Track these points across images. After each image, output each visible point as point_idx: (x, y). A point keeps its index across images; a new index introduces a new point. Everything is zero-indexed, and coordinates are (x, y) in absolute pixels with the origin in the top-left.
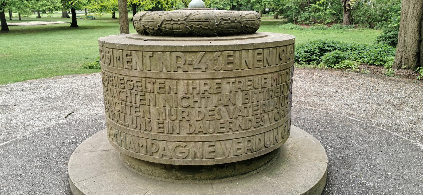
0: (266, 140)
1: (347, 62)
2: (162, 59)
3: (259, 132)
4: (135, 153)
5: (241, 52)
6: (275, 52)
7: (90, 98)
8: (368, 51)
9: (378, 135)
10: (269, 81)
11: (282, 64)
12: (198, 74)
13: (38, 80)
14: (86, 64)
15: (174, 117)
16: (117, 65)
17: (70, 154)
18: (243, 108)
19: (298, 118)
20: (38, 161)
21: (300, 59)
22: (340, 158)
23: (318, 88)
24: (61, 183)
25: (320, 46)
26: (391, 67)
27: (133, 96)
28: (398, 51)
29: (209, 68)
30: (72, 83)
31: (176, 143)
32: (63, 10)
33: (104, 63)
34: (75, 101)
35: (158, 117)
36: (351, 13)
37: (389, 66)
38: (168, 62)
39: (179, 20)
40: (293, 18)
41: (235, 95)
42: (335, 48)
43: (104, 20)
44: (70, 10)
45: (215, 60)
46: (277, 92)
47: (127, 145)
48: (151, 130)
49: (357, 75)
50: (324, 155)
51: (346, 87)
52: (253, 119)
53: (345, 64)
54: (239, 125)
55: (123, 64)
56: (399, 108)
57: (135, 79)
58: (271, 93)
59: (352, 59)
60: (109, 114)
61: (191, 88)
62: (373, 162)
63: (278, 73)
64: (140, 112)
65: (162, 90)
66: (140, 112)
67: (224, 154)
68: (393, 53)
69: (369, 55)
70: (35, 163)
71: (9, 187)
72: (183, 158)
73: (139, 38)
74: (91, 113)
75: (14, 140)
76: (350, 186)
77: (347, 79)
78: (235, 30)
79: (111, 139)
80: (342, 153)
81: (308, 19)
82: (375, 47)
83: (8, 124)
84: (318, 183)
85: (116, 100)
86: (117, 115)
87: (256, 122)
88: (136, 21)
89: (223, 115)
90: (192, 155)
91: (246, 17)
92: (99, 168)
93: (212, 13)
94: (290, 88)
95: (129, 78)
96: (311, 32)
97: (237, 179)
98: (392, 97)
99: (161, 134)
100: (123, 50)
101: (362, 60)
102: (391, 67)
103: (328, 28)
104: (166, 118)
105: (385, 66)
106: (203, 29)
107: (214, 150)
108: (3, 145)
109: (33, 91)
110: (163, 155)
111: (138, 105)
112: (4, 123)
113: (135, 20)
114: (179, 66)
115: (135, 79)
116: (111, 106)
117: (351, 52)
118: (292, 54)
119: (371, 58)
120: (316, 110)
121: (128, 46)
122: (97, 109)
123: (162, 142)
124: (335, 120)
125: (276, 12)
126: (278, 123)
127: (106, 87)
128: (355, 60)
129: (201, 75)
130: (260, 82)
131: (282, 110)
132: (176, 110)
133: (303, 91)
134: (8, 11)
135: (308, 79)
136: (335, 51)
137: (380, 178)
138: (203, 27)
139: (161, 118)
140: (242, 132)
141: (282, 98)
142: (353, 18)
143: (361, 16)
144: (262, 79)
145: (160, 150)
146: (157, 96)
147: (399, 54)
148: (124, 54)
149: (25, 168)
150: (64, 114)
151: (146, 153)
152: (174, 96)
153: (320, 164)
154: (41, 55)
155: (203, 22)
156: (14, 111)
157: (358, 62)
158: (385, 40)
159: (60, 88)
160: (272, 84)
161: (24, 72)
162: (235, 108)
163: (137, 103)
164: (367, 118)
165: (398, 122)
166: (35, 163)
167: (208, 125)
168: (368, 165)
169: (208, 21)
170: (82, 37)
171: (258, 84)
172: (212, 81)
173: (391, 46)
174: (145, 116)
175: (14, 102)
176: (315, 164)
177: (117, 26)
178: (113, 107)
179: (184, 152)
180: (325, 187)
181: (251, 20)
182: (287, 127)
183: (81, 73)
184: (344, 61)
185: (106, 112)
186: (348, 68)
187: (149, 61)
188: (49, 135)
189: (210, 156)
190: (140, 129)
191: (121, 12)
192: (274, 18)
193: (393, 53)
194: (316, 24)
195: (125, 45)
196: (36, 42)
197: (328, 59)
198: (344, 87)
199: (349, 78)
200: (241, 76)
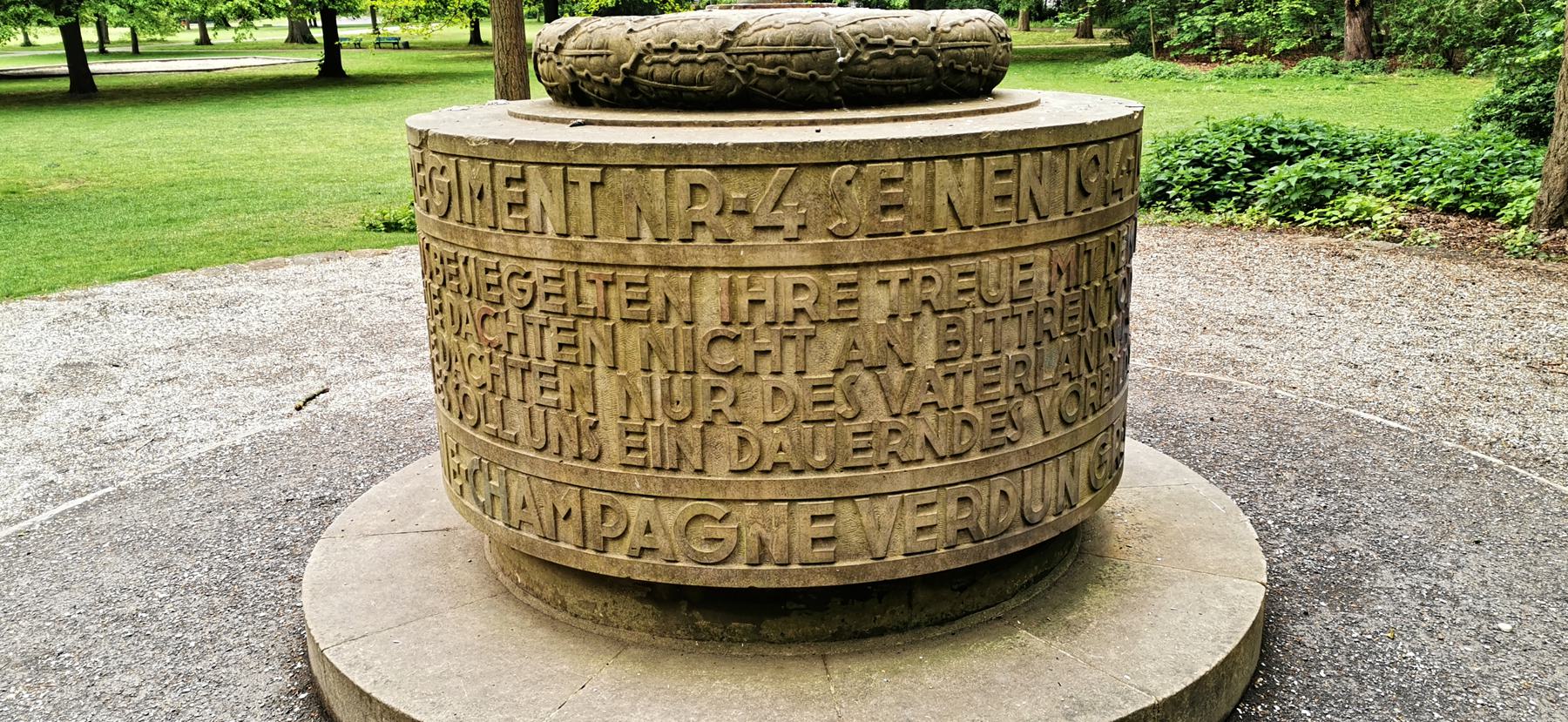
0: (1027, 497)
1: (1353, 201)
2: (635, 192)
3: (1001, 465)
4: (542, 540)
5: (932, 166)
6: (1064, 164)
7: (384, 340)
8: (1437, 159)
9: (1468, 478)
10: (1041, 275)
11: (1090, 209)
12: (773, 249)
13: (201, 274)
14: (374, 215)
15: (682, 411)
16: (473, 217)
17: (311, 542)
18: (940, 375)
19: (1159, 415)
20: (195, 567)
21: (1172, 193)
22: (1317, 566)
23: (1239, 302)
24: (279, 646)
25: (1251, 139)
26: (1527, 221)
27: (532, 333)
28: (1552, 158)
29: (810, 228)
30: (322, 282)
31: (689, 504)
32: (292, 15)
33: (428, 210)
34: (333, 350)
35: (625, 407)
36: (1376, 13)
37: (1518, 216)
38: (659, 206)
39: (700, 47)
40: (1149, 36)
41: (909, 327)
42: (1311, 147)
43: (439, 52)
44: (318, 16)
45: (833, 196)
46: (1071, 318)
47: (513, 511)
48: (599, 457)
49: (1393, 252)
50: (1254, 555)
51: (1347, 297)
52: (980, 419)
53: (1347, 210)
54: (926, 439)
55: (495, 215)
56: (1551, 377)
57: (539, 270)
58: (1047, 319)
59: (1374, 191)
60: (448, 396)
61: (743, 302)
62: (1444, 583)
63: (1073, 245)
64: (557, 389)
65: (639, 309)
66: (557, 389)
67: (869, 545)
68: (1534, 165)
69: (1441, 176)
70: (186, 575)
71: (93, 660)
72: (715, 560)
73: (554, 116)
74: (389, 392)
75: (110, 489)
76: (1351, 672)
77: (1352, 265)
78: (914, 83)
79: (455, 490)
80: (1323, 547)
81: (1209, 38)
82: (1464, 142)
83: (90, 433)
84: (1228, 657)
85: (472, 347)
86: (477, 400)
87: (988, 427)
88: (543, 54)
89: (864, 401)
90: (749, 548)
91: (955, 32)
92: (414, 594)
93: (826, 19)
94: (1122, 300)
95: (519, 263)
96: (1220, 88)
97: (918, 642)
98: (1525, 333)
99: (634, 472)
100: (494, 161)
101: (1413, 194)
102: (1527, 221)
103: (1286, 72)
104: (652, 414)
105: (1503, 214)
106: (791, 79)
107: (831, 530)
108: (72, 509)
109: (182, 314)
110: (643, 549)
111: (550, 363)
112: (75, 429)
113: (541, 50)
114: (702, 220)
115: (539, 270)
116: (454, 367)
117: (1372, 161)
118: (1129, 172)
119: (1449, 185)
120: (1230, 383)
121: (512, 147)
122: (410, 381)
123: (638, 501)
124: (1302, 424)
125: (1083, 12)
126: (1075, 434)
127: (435, 297)
128: (1388, 195)
129: (782, 254)
130: (1005, 279)
131: (1089, 385)
132: (688, 385)
133: (1179, 313)
134: (92, 20)
135: (1202, 267)
136: (1307, 161)
137: (1467, 643)
138: (791, 72)
139: (634, 414)
140: (936, 465)
141: (1088, 338)
142: (1383, 32)
143: (1412, 26)
144: (1012, 268)
145: (631, 529)
146: (619, 330)
147: (1556, 171)
148: (497, 177)
149: (150, 592)
150: (291, 397)
151: (580, 543)
152: (681, 333)
153: (1236, 586)
154: (213, 183)
155: (789, 56)
156: (112, 387)
157: (1398, 202)
158: (1507, 118)
159: (279, 301)
160: (1049, 287)
161: (151, 244)
162: (912, 376)
163: (547, 356)
164: (1428, 417)
165: (1546, 433)
166: (186, 575)
167: (808, 440)
168: (1424, 592)
169: (809, 52)
170: (360, 115)
171: (999, 287)
172: (821, 274)
173: (1528, 141)
174: (577, 403)
175: (112, 352)
176: (1218, 589)
177: (488, 74)
178: (462, 372)
179: (722, 540)
180: (1256, 675)
181: (973, 47)
182: (1108, 447)
183: (356, 247)
184: (1344, 198)
185: (438, 391)
186: (1358, 223)
187: (589, 202)
188: (237, 471)
189: (817, 555)
190: (560, 454)
191: (500, 20)
192: (1076, 36)
193: (1534, 165)
194: (1241, 56)
195: (503, 142)
196: (192, 132)
197: (1281, 192)
198: (1341, 295)
199: (1359, 263)
200: (934, 255)
